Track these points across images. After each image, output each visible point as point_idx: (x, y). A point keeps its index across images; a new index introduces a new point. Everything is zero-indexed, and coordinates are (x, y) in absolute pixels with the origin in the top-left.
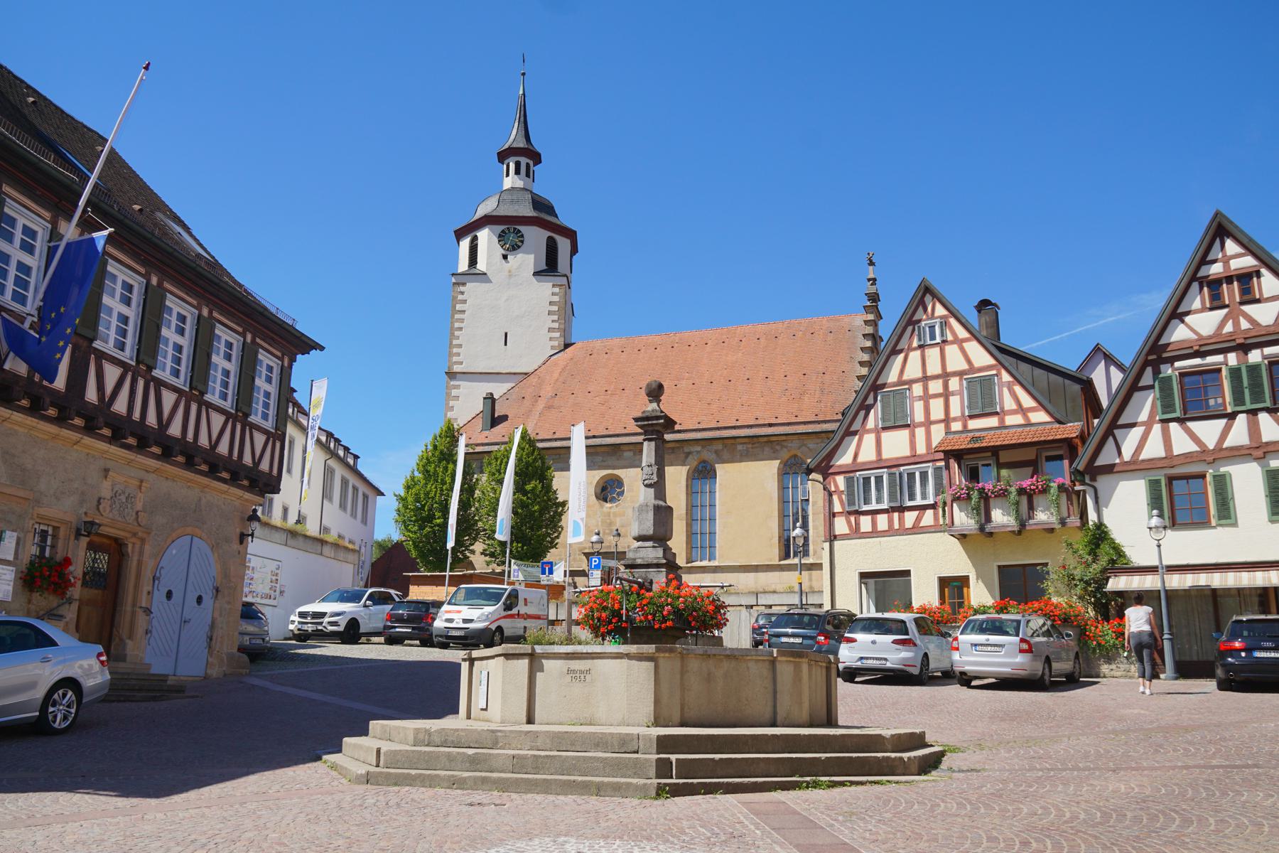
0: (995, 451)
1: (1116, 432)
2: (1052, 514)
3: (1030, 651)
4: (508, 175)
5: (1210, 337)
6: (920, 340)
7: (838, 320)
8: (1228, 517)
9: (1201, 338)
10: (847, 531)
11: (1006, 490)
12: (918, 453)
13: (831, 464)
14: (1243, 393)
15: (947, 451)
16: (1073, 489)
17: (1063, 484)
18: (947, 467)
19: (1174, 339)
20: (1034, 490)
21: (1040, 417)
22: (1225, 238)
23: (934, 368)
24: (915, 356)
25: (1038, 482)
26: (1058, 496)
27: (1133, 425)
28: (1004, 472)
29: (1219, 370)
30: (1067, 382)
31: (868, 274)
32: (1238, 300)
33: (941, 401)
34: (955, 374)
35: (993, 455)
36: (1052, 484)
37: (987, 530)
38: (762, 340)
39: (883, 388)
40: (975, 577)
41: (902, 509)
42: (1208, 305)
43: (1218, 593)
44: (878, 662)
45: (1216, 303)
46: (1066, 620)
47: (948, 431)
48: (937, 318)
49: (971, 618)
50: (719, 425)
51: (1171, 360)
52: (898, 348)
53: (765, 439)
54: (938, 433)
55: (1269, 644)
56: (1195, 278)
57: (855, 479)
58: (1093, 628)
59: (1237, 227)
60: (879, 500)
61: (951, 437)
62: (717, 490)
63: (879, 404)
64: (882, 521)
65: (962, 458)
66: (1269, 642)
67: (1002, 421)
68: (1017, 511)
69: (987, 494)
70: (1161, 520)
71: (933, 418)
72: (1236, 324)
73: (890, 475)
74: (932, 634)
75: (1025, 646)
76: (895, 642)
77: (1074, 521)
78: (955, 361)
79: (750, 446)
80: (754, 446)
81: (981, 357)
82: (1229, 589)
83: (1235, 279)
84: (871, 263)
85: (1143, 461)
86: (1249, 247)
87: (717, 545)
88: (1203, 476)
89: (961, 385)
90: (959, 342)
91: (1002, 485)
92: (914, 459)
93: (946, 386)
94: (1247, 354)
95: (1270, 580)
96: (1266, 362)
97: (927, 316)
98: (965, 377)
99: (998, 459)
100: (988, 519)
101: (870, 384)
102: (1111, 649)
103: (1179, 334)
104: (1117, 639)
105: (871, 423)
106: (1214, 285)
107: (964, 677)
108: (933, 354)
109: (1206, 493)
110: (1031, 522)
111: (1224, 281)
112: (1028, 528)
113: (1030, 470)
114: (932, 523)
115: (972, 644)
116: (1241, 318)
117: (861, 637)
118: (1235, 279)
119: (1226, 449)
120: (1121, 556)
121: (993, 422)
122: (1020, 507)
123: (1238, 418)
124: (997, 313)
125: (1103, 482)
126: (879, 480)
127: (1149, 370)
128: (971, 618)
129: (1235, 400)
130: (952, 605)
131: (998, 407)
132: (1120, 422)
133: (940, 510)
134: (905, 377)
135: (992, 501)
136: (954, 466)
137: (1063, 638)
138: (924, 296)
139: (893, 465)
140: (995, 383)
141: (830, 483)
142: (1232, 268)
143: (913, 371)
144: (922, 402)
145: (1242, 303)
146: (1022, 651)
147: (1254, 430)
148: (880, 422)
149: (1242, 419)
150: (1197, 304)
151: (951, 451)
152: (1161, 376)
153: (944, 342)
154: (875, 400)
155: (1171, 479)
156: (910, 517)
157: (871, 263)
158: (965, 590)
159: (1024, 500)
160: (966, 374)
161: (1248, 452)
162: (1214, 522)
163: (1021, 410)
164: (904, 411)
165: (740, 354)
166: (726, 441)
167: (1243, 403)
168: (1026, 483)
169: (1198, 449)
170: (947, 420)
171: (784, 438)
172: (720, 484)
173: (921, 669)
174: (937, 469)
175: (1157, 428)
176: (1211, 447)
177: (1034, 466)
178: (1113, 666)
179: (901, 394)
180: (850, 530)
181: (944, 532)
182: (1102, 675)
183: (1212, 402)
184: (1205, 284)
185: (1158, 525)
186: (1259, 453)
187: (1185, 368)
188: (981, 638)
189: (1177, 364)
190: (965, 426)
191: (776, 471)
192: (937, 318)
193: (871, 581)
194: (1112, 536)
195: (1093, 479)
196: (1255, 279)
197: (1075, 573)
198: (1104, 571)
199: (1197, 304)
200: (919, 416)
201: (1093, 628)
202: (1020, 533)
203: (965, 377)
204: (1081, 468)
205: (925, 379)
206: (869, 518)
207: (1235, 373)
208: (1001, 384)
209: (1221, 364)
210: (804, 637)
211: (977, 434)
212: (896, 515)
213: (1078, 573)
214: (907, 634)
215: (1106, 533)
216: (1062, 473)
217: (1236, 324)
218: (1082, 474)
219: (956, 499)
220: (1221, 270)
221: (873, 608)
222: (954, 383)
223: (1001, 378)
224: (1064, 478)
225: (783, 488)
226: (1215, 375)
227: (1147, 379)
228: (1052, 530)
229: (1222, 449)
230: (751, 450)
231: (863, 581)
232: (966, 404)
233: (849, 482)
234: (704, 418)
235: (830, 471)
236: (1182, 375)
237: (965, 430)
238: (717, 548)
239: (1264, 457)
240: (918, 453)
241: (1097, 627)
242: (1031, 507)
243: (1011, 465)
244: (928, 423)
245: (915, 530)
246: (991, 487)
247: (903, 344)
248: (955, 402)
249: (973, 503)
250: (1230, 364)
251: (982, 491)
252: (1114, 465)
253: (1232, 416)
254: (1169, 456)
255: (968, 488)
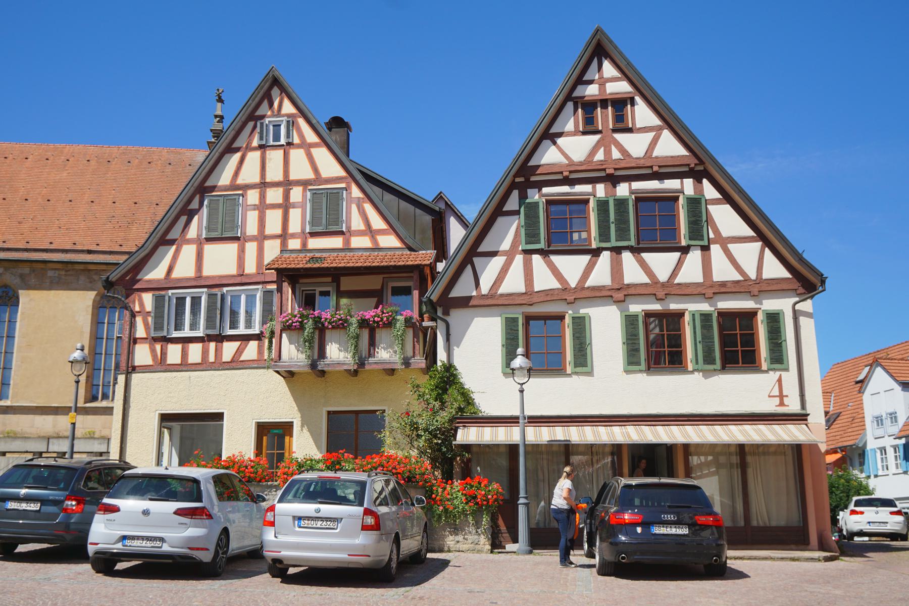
0: (336, 274)
1: (476, 260)
2: (395, 352)
3: (376, 527)
4: (349, 555)
5: (581, 164)
6: (261, 138)
7: (180, 153)
8: (584, 365)
9: (571, 163)
10: (149, 361)
11: (346, 321)
12: (246, 271)
13: (138, 277)
14: (609, 228)
15: (281, 269)
16: (421, 325)
17: (411, 318)
18: (280, 290)
19: (544, 161)
20: (378, 322)
21: (390, 241)
22: (603, 58)
23: (275, 173)
24: (254, 157)
25: (383, 313)
26: (404, 331)
27: (494, 254)
28: (344, 301)
29: (587, 202)
30: (418, 211)
31: (216, 111)
32: (611, 127)
33: (279, 213)
34: (298, 183)
35: (333, 281)
36: (398, 317)
37: (320, 368)
38: (93, 163)
39: (212, 192)
40: (300, 423)
41: (220, 339)
42: (581, 129)
43: (747, 449)
44: (149, 544)
45: (589, 128)
46: (410, 479)
47: (284, 249)
48: (283, 116)
49: (296, 477)
50: (29, 246)
51: (539, 185)
52: (235, 145)
53: (81, 267)
54: (272, 250)
55: (671, 517)
56: (570, 98)
57: (167, 298)
58: (440, 490)
59: (616, 47)
60: (194, 326)
61: (286, 255)
62: (18, 319)
63: (205, 210)
64: (195, 352)
65: (298, 283)
66: (670, 513)
67: (347, 242)
68: (356, 346)
69: (323, 325)
70: (527, 360)
71: (268, 231)
72: (608, 153)
73: (211, 296)
74: (238, 499)
75: (370, 520)
76: (179, 512)
77: (420, 362)
78: (300, 169)
79: (63, 273)
80: (69, 273)
81: (330, 167)
82: (498, 445)
83: (609, 104)
84: (220, 100)
85: (502, 295)
86: (626, 72)
87: (12, 382)
88: (561, 318)
89: (304, 196)
90: (307, 147)
91: (342, 313)
92: (241, 280)
93: (286, 196)
94: (615, 187)
95: (629, 436)
96: (633, 197)
97: (273, 112)
98: (310, 187)
99: (338, 286)
100: (322, 354)
101: (196, 184)
102: (460, 516)
103: (550, 156)
104: (467, 503)
105: (192, 232)
106: (589, 106)
107: (278, 566)
108: (275, 157)
109: (562, 337)
110: (371, 360)
111: (599, 105)
112: (367, 367)
113: (374, 300)
114: (255, 358)
115: (294, 517)
116: (613, 147)
117: (130, 505)
118: (609, 104)
119: (588, 288)
120: (469, 404)
121: (336, 242)
122: (360, 343)
123: (602, 255)
124: (348, 135)
125: (456, 316)
126: (196, 301)
127: (515, 194)
128: (296, 477)
129: (600, 235)
130: (270, 457)
131: (344, 225)
132: (480, 250)
133: (266, 342)
134: (240, 181)
135: (328, 334)
136: (288, 290)
137: (413, 505)
138: (270, 88)
139: (215, 284)
140: (343, 198)
141: (134, 302)
142: (608, 92)
143: (250, 173)
144: (257, 212)
145: (615, 131)
146: (365, 528)
147: (617, 270)
148: (204, 232)
149: (606, 256)
150: (570, 126)
151: (285, 269)
152: (527, 201)
153: (289, 144)
154: (201, 204)
155: (528, 318)
156: (229, 349)
157: (220, 100)
158: (287, 439)
159: (365, 334)
160: (311, 185)
161: (609, 293)
162: (569, 371)
163: (370, 231)
164: (233, 220)
165: (65, 174)
166: (35, 265)
167: (608, 240)
168: (370, 314)
169: (560, 286)
170: (284, 236)
171: (104, 267)
172: (23, 314)
173: (216, 553)
174: (267, 294)
175: (519, 259)
176: (573, 285)
177: (378, 296)
178: (460, 538)
179: (232, 203)
180: (153, 360)
181: (268, 368)
182: (446, 549)
183: (576, 236)
184: (580, 106)
185: (523, 366)
186: (619, 296)
187: (553, 195)
188: (308, 508)
189: (545, 190)
190: (304, 244)
191: (91, 303)
192: (283, 116)
193: (176, 426)
194: (461, 380)
195: (446, 313)
196: (629, 106)
197: (420, 421)
198: (452, 420)
199: (570, 126)
200: (252, 228)
201: (440, 490)
202: (356, 372)
203: (310, 187)
204: (434, 297)
205: (263, 185)
206: (179, 347)
207: (603, 205)
208: (350, 200)
209: (589, 194)
210: (43, 501)
211: (318, 255)
212: (212, 345)
213: (422, 422)
214: (200, 500)
215: (455, 376)
216: (412, 306)
217: (608, 153)
218: (433, 306)
219: (287, 328)
220: (597, 93)
221: (175, 459)
222: (296, 194)
223: (351, 193)
224: (412, 311)
225: (97, 322)
226: (581, 207)
227: (513, 203)
228: (392, 372)
229: (583, 289)
230: (63, 277)
231: (163, 424)
232: (308, 218)
233: (159, 302)
234: (11, 237)
235: (135, 287)
236: (549, 203)
237: (304, 249)
238: (11, 386)
239: (624, 301)
240: (246, 271)
241: (444, 489)
242: (372, 343)
243: (353, 294)
244: (262, 237)
245: (233, 364)
246: (329, 316)
247: (241, 142)
248: (295, 215)
249: (306, 334)
250: (598, 195)
251: (317, 321)
252: (470, 298)
253: (596, 253)
254: (530, 291)
255: (302, 316)
